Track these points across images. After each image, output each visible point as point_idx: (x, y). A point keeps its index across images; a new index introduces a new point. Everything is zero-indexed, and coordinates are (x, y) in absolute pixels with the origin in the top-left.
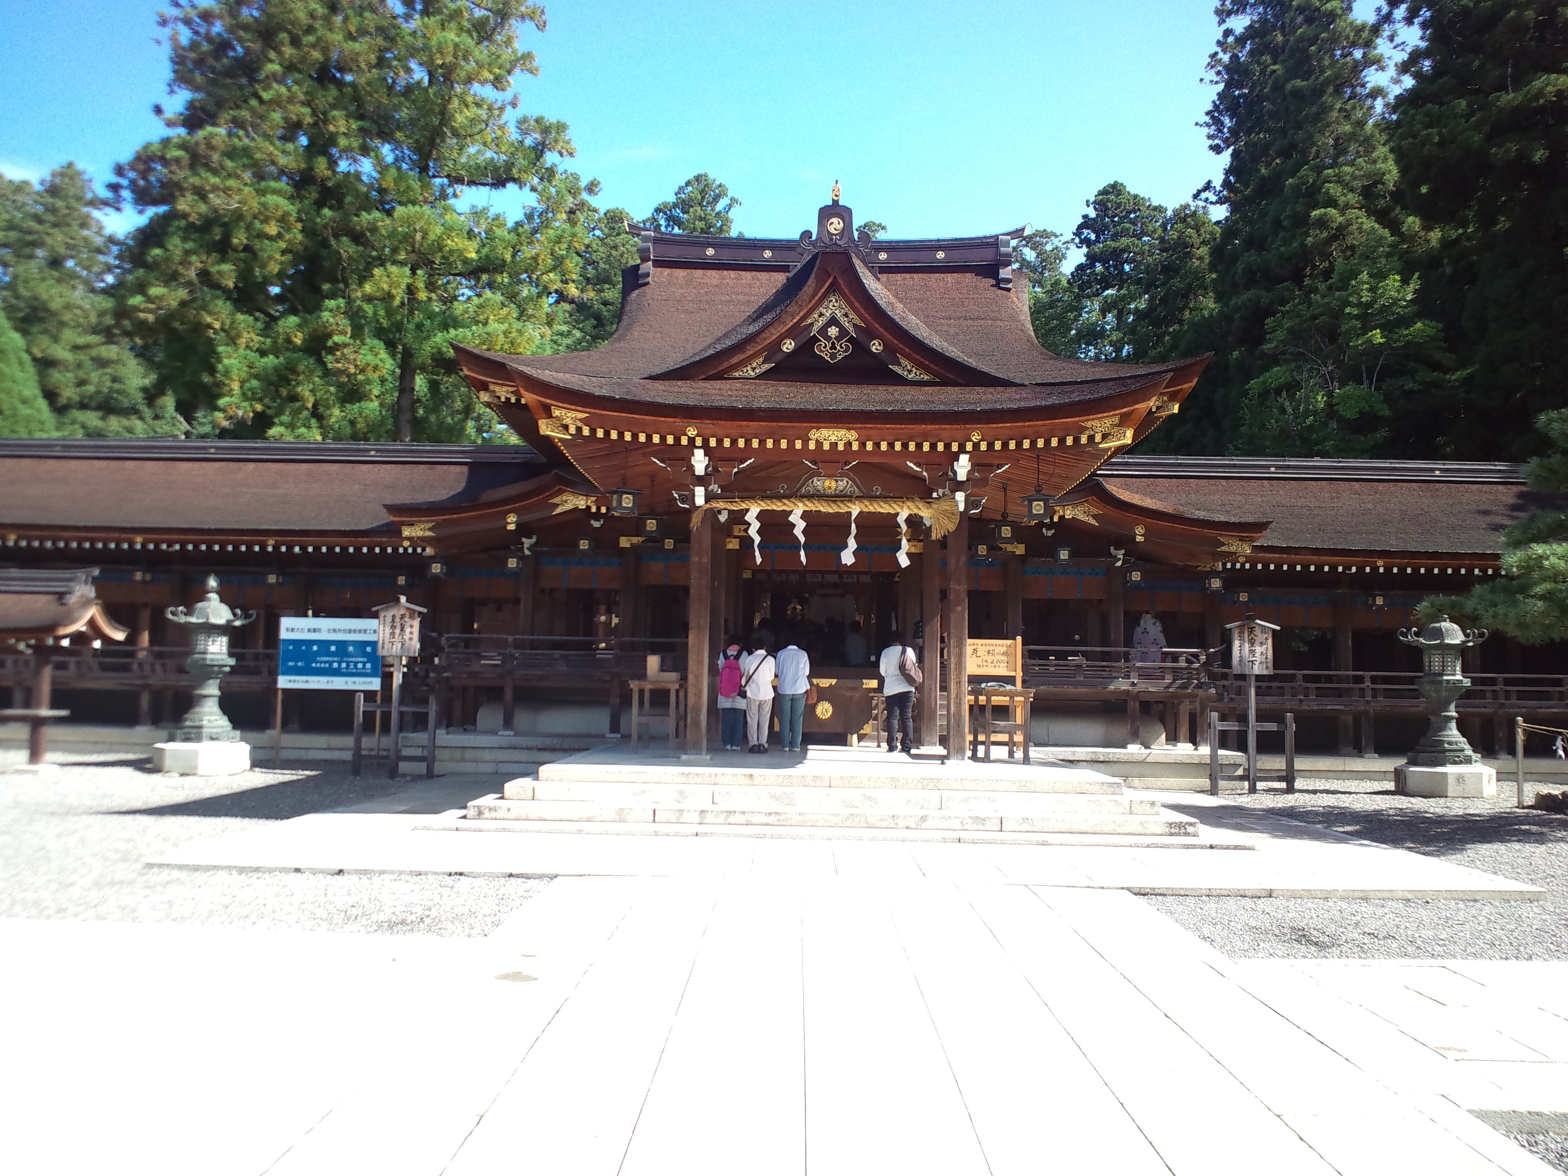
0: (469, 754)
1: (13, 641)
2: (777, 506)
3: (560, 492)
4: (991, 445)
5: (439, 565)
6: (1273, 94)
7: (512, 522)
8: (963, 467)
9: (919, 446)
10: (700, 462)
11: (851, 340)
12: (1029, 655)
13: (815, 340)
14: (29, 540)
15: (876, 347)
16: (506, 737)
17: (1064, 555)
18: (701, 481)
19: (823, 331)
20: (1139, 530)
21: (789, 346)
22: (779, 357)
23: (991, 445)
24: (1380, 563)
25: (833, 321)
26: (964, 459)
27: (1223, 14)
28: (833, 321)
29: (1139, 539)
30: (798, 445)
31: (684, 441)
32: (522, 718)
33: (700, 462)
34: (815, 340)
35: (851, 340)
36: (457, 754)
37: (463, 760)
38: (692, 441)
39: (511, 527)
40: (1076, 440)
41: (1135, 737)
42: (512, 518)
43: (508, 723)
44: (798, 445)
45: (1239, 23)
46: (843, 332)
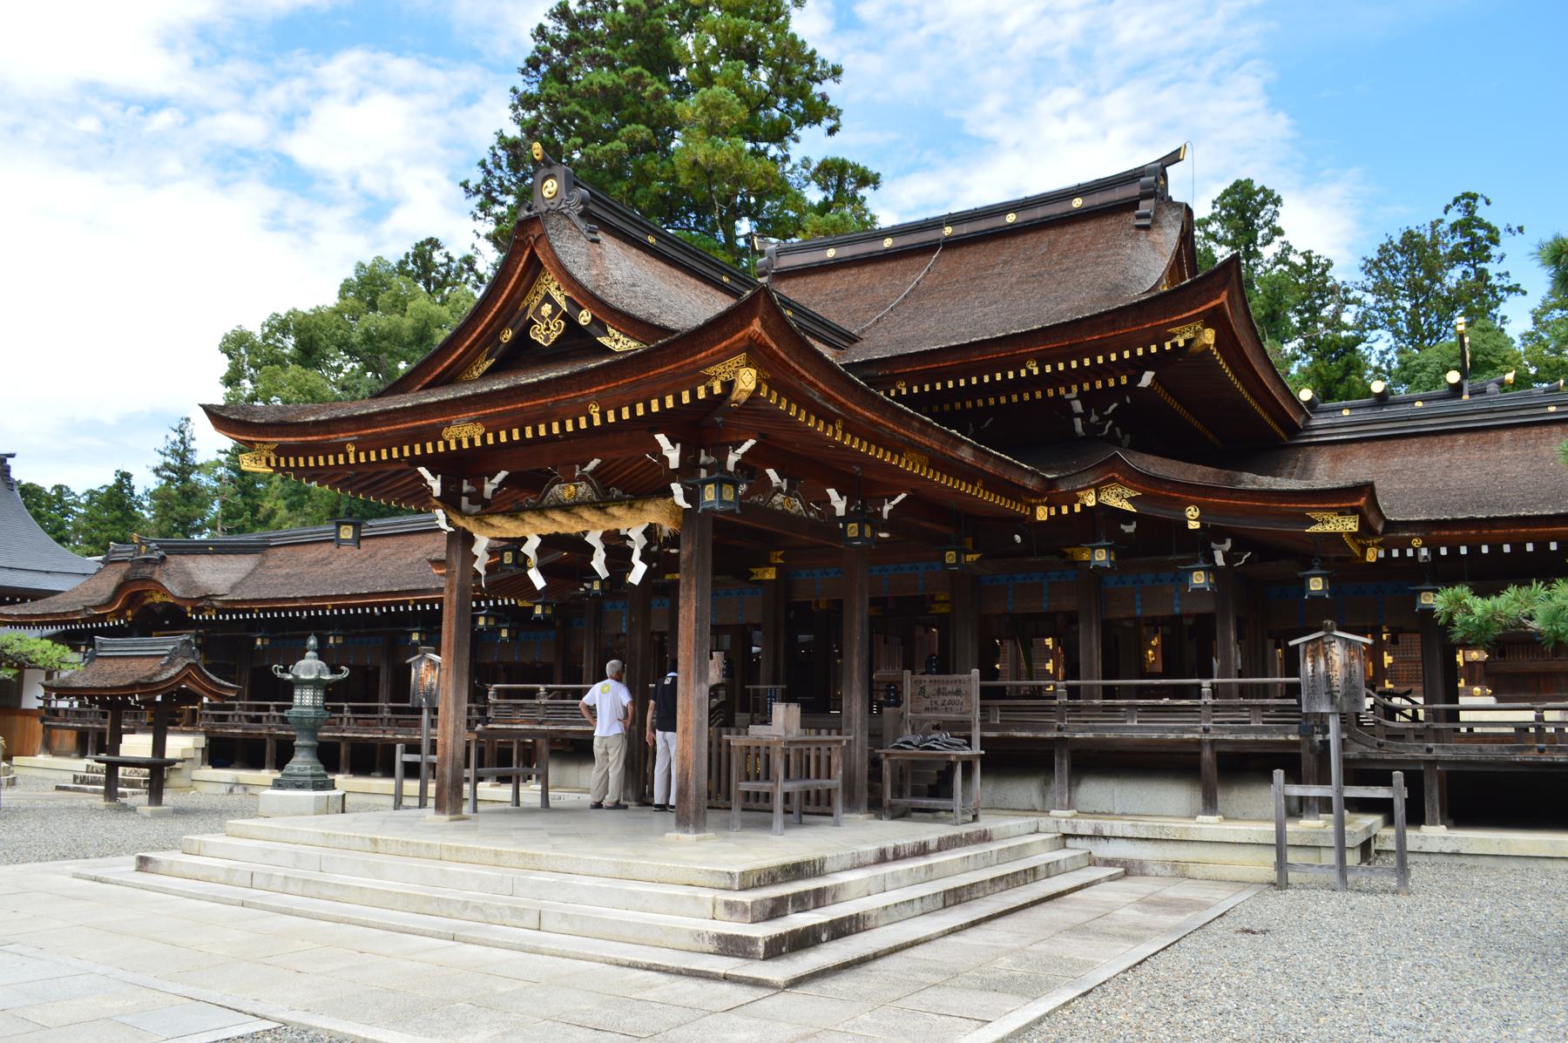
15: (584, 318)
20: (1192, 513)
21: (507, 335)
46: (556, 307)
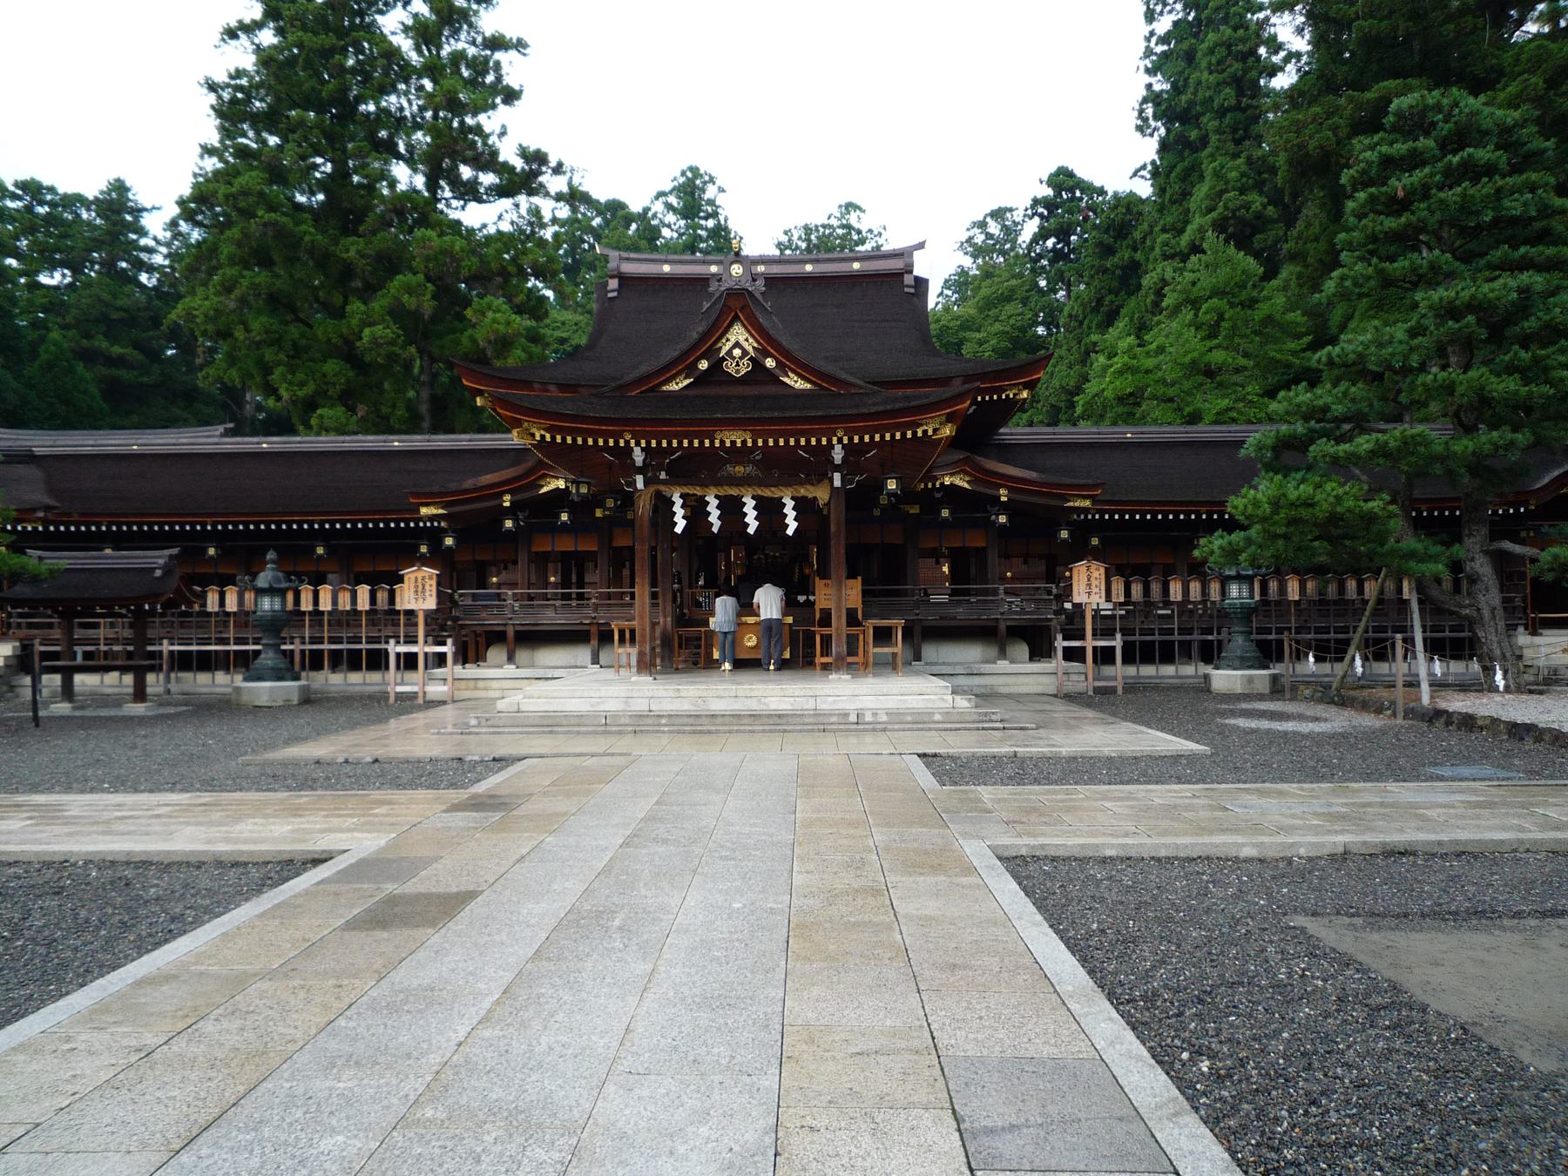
0: (481, 684)
1: (98, 221)
2: (698, 491)
3: (545, 476)
4: (851, 439)
5: (1098, 572)
6: (1201, 86)
7: (507, 502)
8: (838, 454)
9: (808, 441)
10: (638, 457)
11: (751, 359)
12: (865, 593)
13: (723, 359)
14: (119, 525)
15: (770, 363)
16: (510, 670)
17: (945, 513)
18: (640, 471)
19: (730, 352)
22: (697, 374)
23: (851, 439)
24: (1423, 507)
25: (737, 345)
26: (838, 448)
27: (1150, 16)
28: (737, 345)
29: (1004, 499)
30: (707, 443)
31: (622, 443)
32: (522, 655)
33: (638, 457)
34: (723, 359)
35: (751, 359)
36: (471, 684)
37: (476, 688)
38: (627, 443)
39: (507, 504)
40: (915, 433)
41: (1003, 654)
42: (507, 497)
43: (511, 659)
44: (707, 443)
45: (1164, 25)
46: (745, 353)
